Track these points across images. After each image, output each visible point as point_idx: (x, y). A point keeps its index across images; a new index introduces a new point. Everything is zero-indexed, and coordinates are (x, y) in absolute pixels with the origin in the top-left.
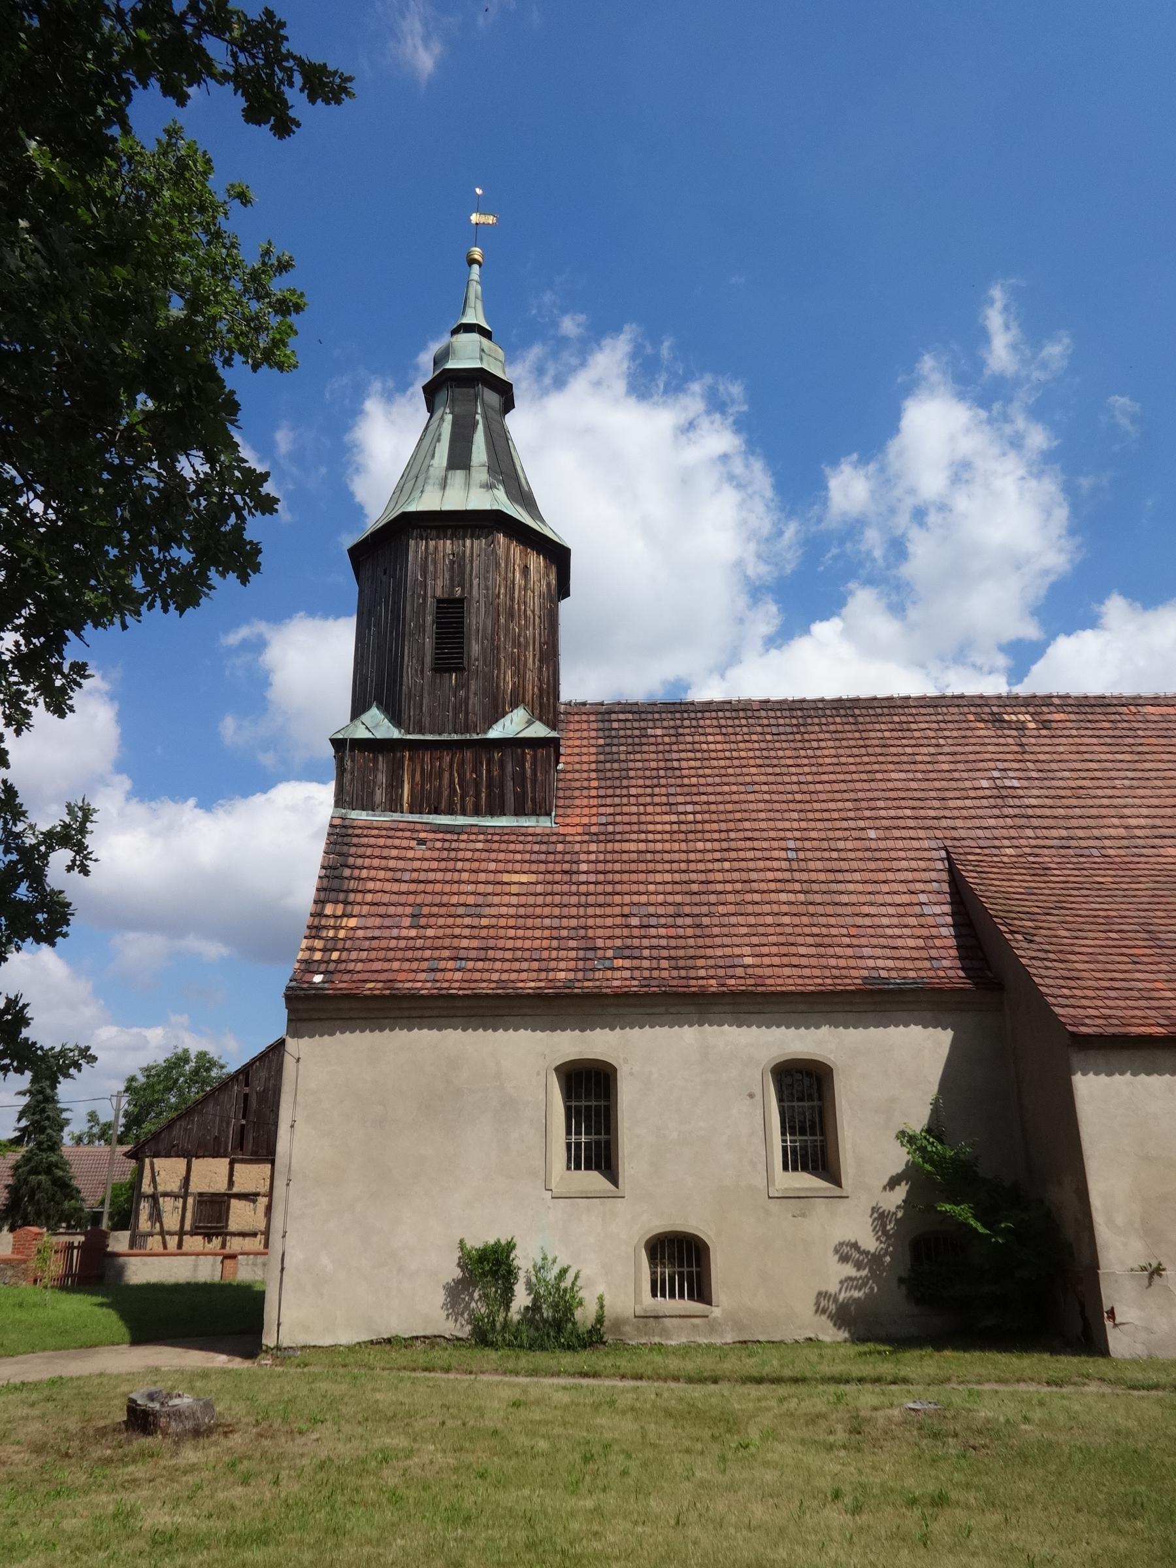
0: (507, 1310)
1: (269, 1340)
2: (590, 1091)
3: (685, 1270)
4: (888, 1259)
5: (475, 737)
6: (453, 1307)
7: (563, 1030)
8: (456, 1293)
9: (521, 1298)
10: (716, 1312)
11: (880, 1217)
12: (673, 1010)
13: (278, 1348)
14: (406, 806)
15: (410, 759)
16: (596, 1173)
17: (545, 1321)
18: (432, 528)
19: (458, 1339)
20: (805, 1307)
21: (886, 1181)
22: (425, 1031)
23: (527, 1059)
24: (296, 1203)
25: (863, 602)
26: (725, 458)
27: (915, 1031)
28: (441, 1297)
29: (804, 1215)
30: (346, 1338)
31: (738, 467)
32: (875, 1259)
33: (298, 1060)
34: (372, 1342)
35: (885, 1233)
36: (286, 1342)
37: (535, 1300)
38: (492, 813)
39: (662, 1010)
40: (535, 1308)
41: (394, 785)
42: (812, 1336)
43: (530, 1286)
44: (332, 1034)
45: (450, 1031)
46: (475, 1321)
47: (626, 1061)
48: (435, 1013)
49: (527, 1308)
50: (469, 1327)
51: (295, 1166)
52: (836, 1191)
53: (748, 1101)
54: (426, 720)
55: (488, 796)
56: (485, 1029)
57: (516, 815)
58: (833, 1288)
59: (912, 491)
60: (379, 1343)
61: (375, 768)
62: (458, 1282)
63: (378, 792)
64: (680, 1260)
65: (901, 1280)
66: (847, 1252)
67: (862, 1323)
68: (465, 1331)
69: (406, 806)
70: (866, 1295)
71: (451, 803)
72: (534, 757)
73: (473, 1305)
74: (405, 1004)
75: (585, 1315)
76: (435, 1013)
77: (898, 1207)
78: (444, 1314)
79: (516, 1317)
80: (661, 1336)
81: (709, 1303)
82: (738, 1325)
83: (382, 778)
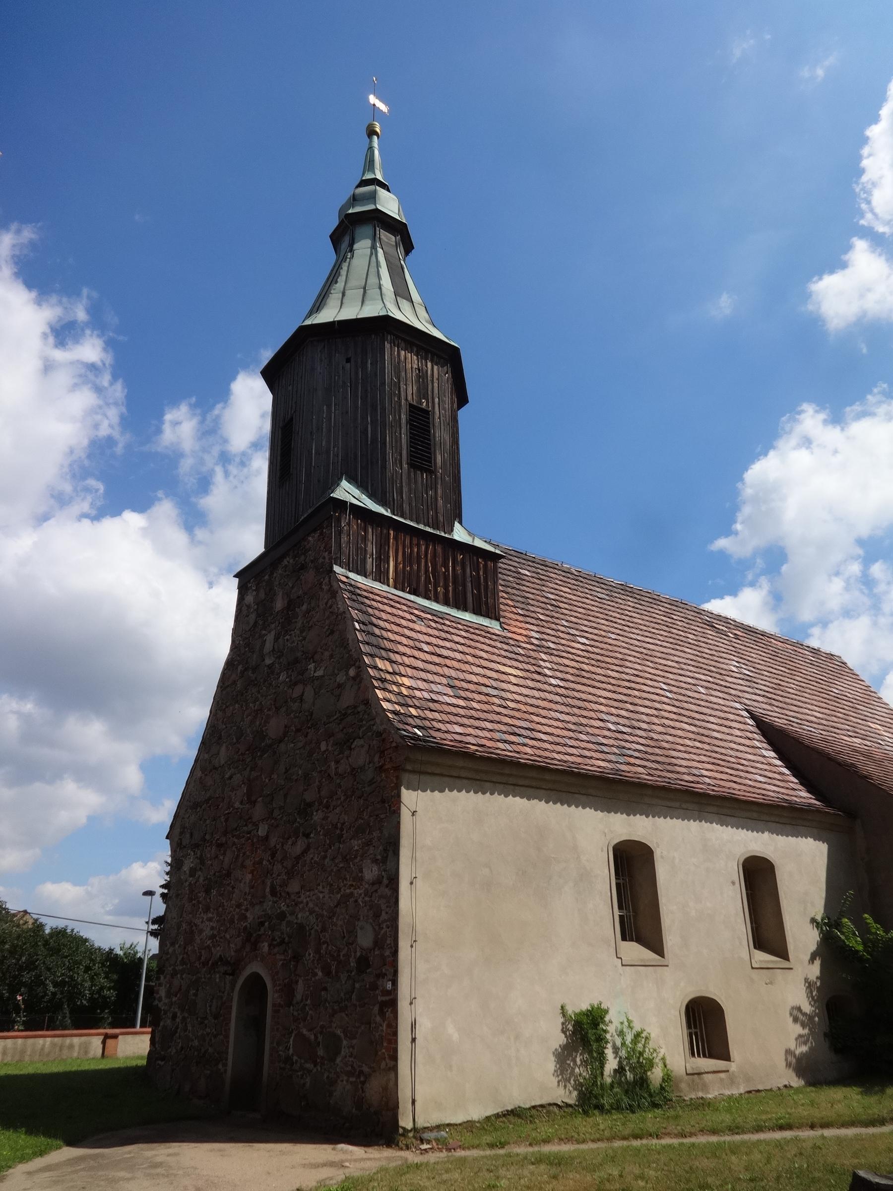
0: (603, 1078)
1: (406, 1122)
2: (633, 867)
3: (693, 1030)
4: (817, 1019)
5: (443, 534)
6: (562, 1074)
7: (616, 813)
8: (563, 1056)
9: (611, 1064)
10: (733, 1067)
11: (809, 985)
12: (684, 806)
13: (415, 1129)
14: (391, 581)
15: (396, 538)
16: (634, 943)
17: (627, 1082)
18: (403, 339)
19: (568, 1105)
20: (780, 1061)
21: (809, 957)
22: (518, 798)
23: (593, 832)
24: (421, 967)
25: (166, 509)
26: (92, 367)
27: (810, 840)
28: (551, 1065)
29: (771, 983)
30: (476, 1113)
31: (105, 379)
32: (811, 1018)
33: (414, 813)
34: (497, 1116)
35: (813, 997)
36: (421, 1123)
37: (620, 1063)
38: (458, 607)
39: (677, 804)
40: (620, 1070)
41: (382, 559)
42: (787, 1083)
43: (616, 1050)
44: (442, 791)
45: (536, 801)
46: (578, 1086)
47: (658, 846)
48: (527, 782)
49: (615, 1070)
50: (575, 1093)
51: (419, 927)
52: (785, 964)
53: (731, 887)
54: (406, 507)
55: (454, 590)
56: (562, 804)
57: (475, 613)
58: (792, 1045)
59: (226, 441)
60: (504, 1115)
61: (365, 539)
62: (564, 1047)
63: (369, 561)
64: (705, 1023)
65: (825, 1035)
66: (796, 1014)
67: (810, 1071)
68: (572, 1098)
69: (391, 581)
70: (810, 1048)
71: (427, 590)
72: (485, 566)
73: (577, 1070)
74: (507, 771)
75: (656, 1075)
76: (527, 782)
77: (817, 978)
78: (555, 1080)
79: (608, 1080)
80: (702, 1090)
81: (726, 1057)
82: (748, 1079)
83: (372, 548)
